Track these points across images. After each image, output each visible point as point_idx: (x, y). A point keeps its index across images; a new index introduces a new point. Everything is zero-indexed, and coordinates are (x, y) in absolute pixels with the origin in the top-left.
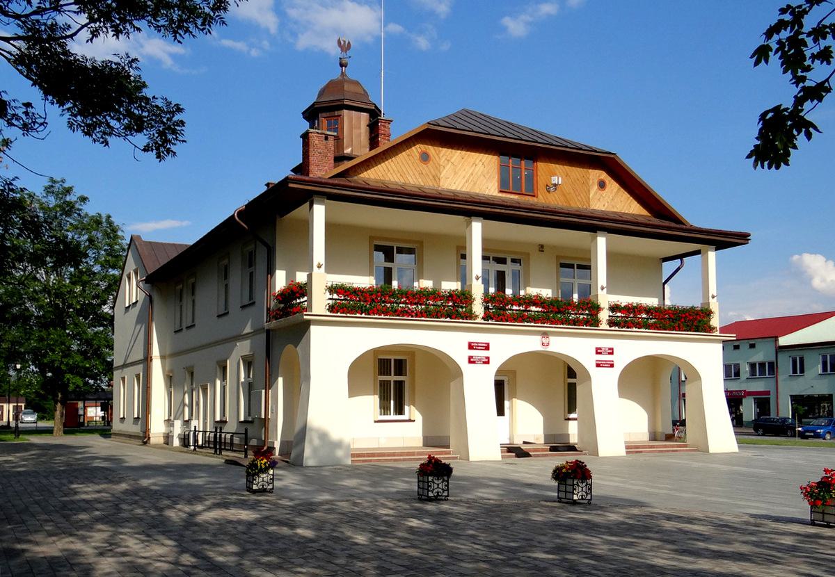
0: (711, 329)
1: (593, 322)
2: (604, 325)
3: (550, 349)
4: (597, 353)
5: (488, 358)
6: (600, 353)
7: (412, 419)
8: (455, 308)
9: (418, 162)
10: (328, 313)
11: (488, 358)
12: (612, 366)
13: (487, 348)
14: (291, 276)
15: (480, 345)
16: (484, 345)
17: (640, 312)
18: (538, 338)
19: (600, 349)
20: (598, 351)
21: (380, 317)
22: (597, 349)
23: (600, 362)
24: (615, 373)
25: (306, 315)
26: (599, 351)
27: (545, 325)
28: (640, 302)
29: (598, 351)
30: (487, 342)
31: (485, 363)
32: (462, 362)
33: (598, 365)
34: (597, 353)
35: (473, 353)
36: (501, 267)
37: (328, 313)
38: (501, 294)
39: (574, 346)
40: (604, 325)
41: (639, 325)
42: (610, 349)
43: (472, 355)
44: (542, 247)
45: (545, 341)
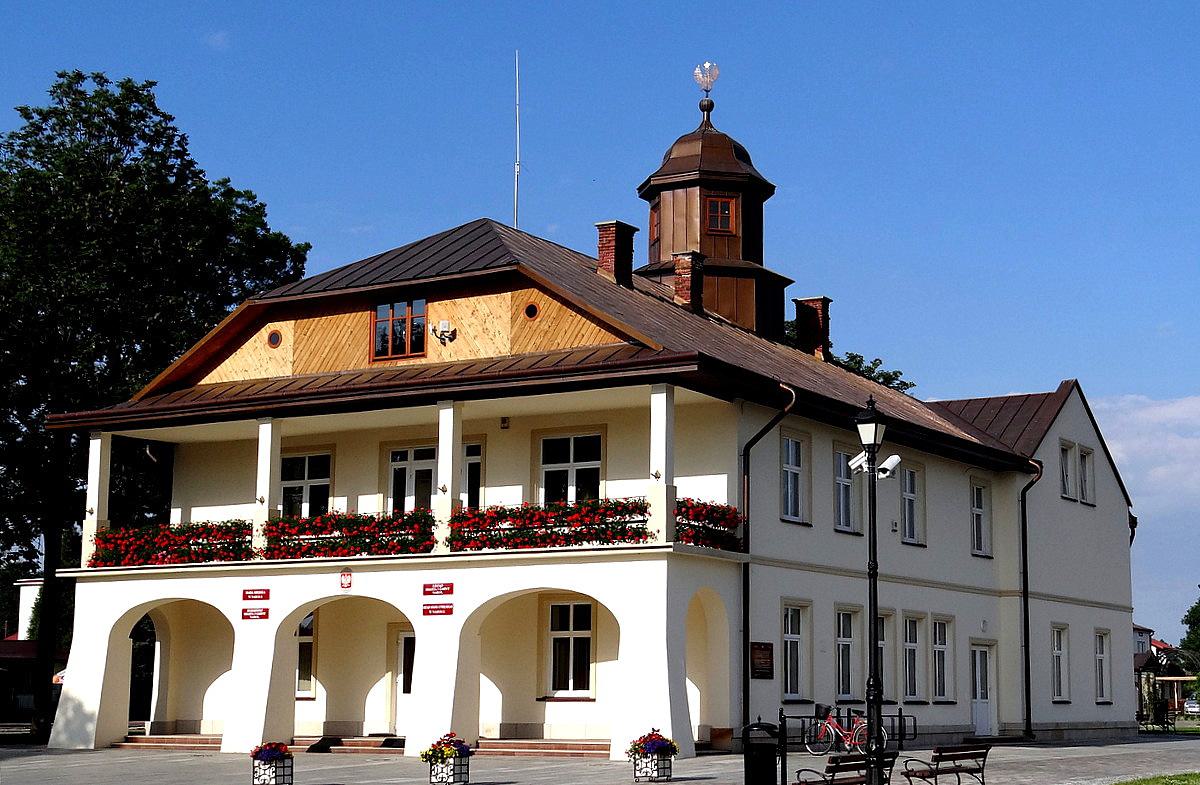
0: (250, 554)
1: (425, 543)
2: (441, 548)
3: (354, 592)
4: (425, 593)
5: (266, 610)
6: (430, 593)
7: (592, 697)
8: (231, 544)
9: (267, 346)
10: (90, 569)
11: (266, 610)
12: (449, 612)
13: (266, 595)
14: (186, 514)
15: (256, 593)
16: (262, 592)
17: (525, 517)
18: (336, 578)
19: (430, 586)
20: (427, 590)
21: (554, 549)
22: (425, 586)
23: (429, 607)
24: (453, 626)
25: (670, 547)
26: (427, 590)
27: (314, 559)
28: (501, 505)
29: (427, 590)
30: (266, 588)
31: (261, 617)
32: (233, 616)
33: (426, 612)
34: (425, 593)
35: (248, 604)
36: (400, 465)
37: (265, 561)
38: (587, 500)
39: (393, 584)
40: (441, 548)
41: (494, 543)
42: (445, 585)
43: (245, 607)
44: (504, 420)
45: (346, 580)
